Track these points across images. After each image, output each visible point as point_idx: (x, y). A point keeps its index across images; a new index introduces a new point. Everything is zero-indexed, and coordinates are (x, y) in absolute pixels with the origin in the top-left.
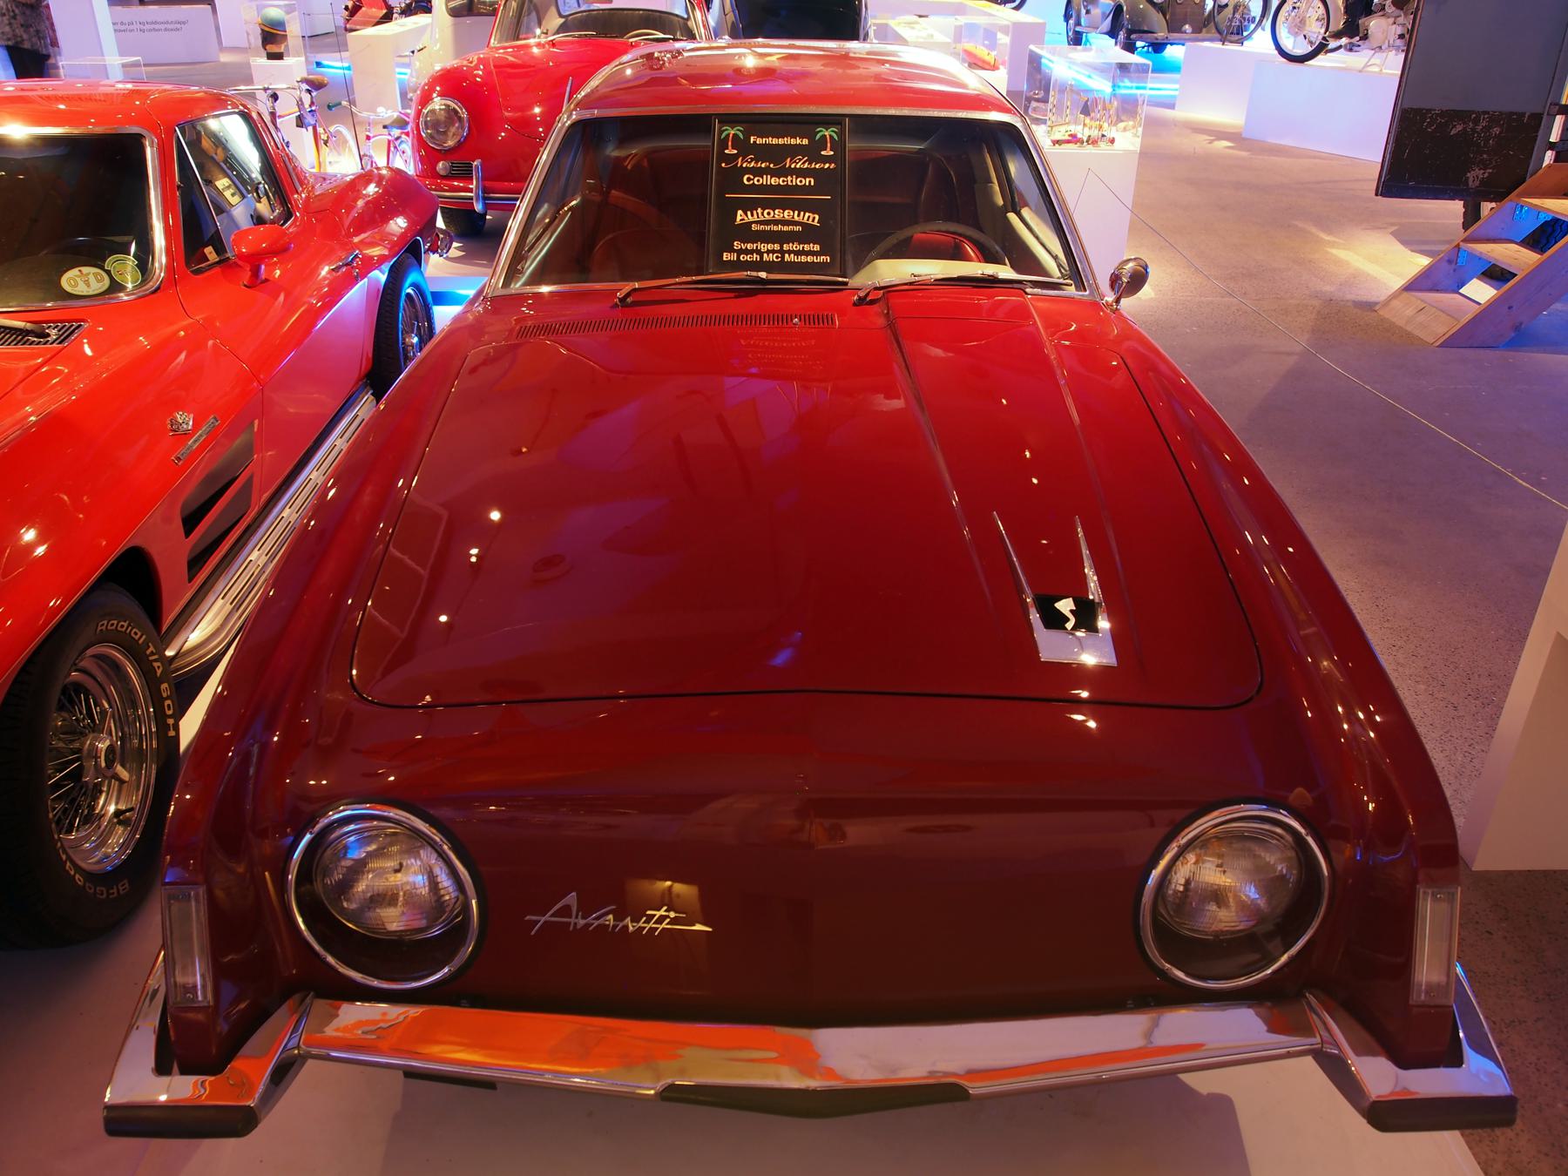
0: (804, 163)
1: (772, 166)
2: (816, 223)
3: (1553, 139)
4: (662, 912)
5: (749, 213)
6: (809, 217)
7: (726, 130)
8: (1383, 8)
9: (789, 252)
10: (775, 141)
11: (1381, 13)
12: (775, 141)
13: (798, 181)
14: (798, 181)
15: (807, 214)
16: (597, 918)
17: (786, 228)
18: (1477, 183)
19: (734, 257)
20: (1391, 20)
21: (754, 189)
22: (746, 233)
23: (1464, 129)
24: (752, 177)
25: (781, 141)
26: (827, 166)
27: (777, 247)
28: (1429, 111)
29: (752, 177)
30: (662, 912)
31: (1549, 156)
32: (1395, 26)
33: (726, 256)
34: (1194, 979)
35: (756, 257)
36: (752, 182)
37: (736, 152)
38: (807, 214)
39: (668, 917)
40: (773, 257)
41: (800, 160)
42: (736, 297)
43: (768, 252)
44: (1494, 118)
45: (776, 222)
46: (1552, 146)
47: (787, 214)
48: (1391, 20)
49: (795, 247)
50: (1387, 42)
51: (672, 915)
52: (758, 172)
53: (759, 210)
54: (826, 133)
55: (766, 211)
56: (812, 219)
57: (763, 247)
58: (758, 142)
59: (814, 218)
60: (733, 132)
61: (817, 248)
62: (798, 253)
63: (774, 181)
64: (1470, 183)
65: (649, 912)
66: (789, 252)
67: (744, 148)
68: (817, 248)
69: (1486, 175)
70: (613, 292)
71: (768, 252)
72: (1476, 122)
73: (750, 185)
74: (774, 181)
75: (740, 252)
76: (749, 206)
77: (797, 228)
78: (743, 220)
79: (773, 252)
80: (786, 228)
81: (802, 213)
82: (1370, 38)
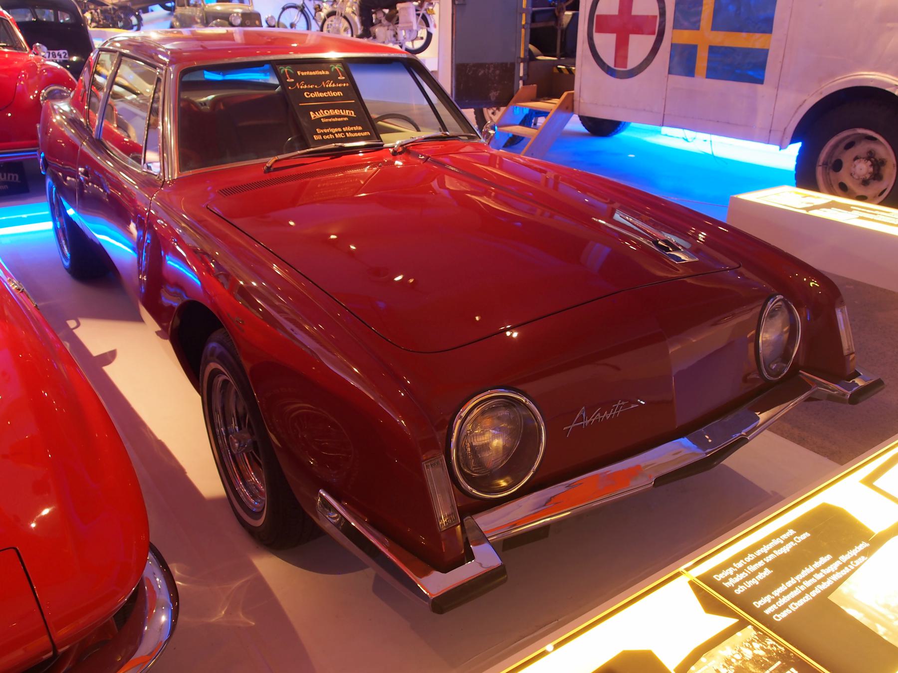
0: (332, 84)
1: (316, 86)
2: (353, 115)
3: (521, 74)
4: (619, 404)
5: (316, 113)
6: (11, 177)
7: (282, 69)
8: (380, 22)
9: (348, 132)
10: (311, 73)
11: (379, 24)
12: (311, 73)
13: (334, 94)
14: (334, 94)
15: (9, 175)
16: (594, 418)
17: (339, 119)
18: (494, 98)
19: (320, 137)
20: (386, 28)
21: (311, 100)
22: (318, 123)
23: (484, 72)
24: (309, 93)
25: (314, 73)
26: (344, 85)
27: (340, 130)
28: (468, 64)
29: (309, 93)
30: (619, 404)
31: (521, 82)
32: (389, 31)
33: (316, 138)
34: (480, 493)
35: (331, 136)
36: (310, 96)
37: (293, 80)
38: (9, 175)
39: (622, 405)
40: (340, 135)
41: (330, 83)
42: (331, 159)
43: (337, 133)
44: (497, 66)
45: (334, 117)
46: (521, 78)
47: (336, 112)
48: (386, 28)
49: (349, 129)
50: (387, 39)
51: (623, 403)
52: (312, 91)
53: (321, 111)
54: (336, 68)
55: (325, 111)
56: (352, 114)
57: (334, 130)
58: (302, 74)
59: (15, 177)
60: (286, 70)
61: (360, 128)
62: (353, 132)
63: (321, 95)
64: (492, 98)
65: (614, 406)
66: (348, 132)
67: (299, 79)
68: (360, 128)
69: (497, 94)
70: (264, 164)
71: (337, 133)
72: (489, 69)
73: (308, 98)
74: (321, 95)
75: (322, 134)
76: (316, 109)
77: (346, 119)
78: (315, 117)
79: (340, 133)
80: (339, 119)
81: (5, 175)
82: (378, 38)
